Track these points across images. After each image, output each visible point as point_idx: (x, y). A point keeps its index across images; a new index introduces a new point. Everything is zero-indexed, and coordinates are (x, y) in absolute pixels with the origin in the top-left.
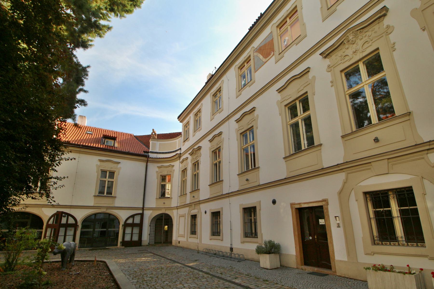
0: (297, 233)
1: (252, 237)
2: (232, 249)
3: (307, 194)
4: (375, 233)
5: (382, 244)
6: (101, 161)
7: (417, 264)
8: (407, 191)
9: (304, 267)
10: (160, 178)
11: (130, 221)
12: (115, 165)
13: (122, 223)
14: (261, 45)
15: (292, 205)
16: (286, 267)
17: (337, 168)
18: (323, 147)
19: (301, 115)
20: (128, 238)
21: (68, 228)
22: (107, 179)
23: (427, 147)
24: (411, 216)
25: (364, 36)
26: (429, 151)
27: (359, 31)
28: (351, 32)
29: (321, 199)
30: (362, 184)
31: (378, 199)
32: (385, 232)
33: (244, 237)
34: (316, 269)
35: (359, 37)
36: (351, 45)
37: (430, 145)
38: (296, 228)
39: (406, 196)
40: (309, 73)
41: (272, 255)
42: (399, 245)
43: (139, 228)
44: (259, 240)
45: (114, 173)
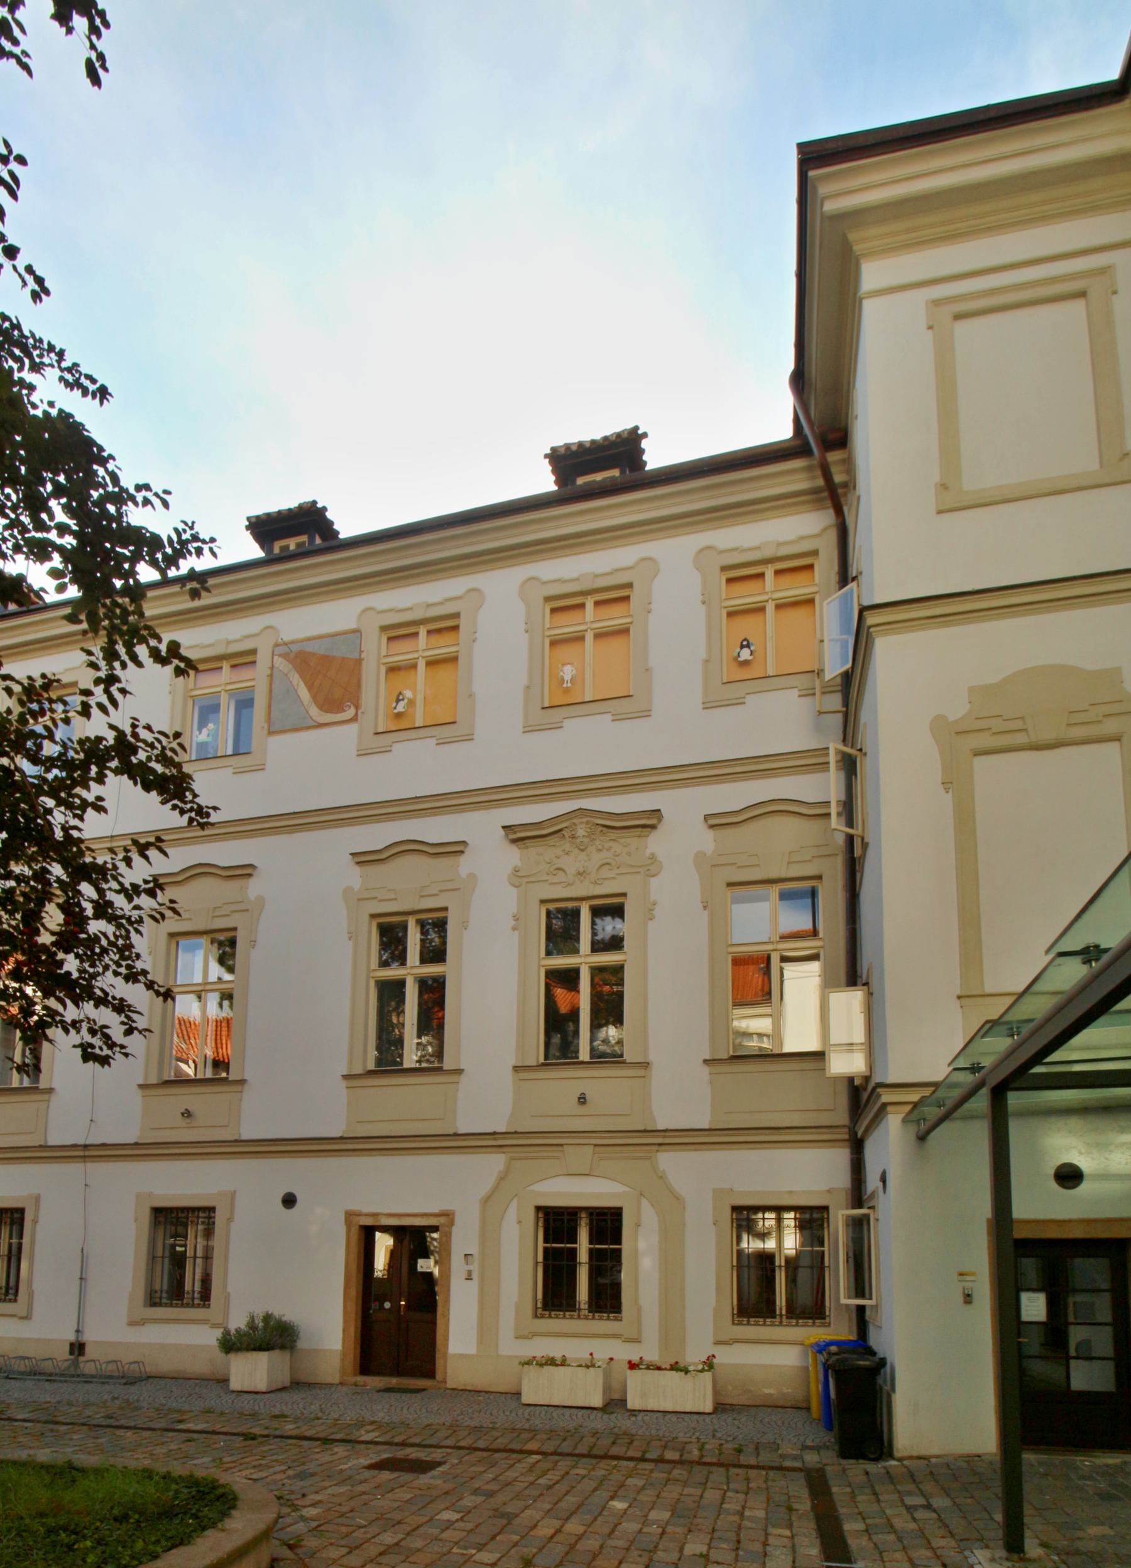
0: (353, 1292)
1: (182, 1306)
2: (78, 1348)
3: (400, 1190)
4: (540, 1295)
5: (550, 1317)
7: (603, 1350)
8: (612, 1214)
9: (361, 1379)
14: (311, 648)
16: (309, 1385)
18: (463, 1078)
19: (413, 969)
22: (584, 959)
23: (660, 1141)
24: (565, 1263)
25: (607, 845)
26: (663, 1148)
27: (601, 828)
28: (585, 820)
29: (436, 1211)
31: (557, 1223)
32: (556, 1294)
33: (145, 1306)
34: (394, 1381)
35: (597, 842)
36: (576, 851)
37: (664, 1137)
38: (354, 1280)
39: (608, 1223)
40: (463, 859)
41: (276, 1354)
42: (579, 1317)
43: (1105, 1262)
44: (214, 1311)
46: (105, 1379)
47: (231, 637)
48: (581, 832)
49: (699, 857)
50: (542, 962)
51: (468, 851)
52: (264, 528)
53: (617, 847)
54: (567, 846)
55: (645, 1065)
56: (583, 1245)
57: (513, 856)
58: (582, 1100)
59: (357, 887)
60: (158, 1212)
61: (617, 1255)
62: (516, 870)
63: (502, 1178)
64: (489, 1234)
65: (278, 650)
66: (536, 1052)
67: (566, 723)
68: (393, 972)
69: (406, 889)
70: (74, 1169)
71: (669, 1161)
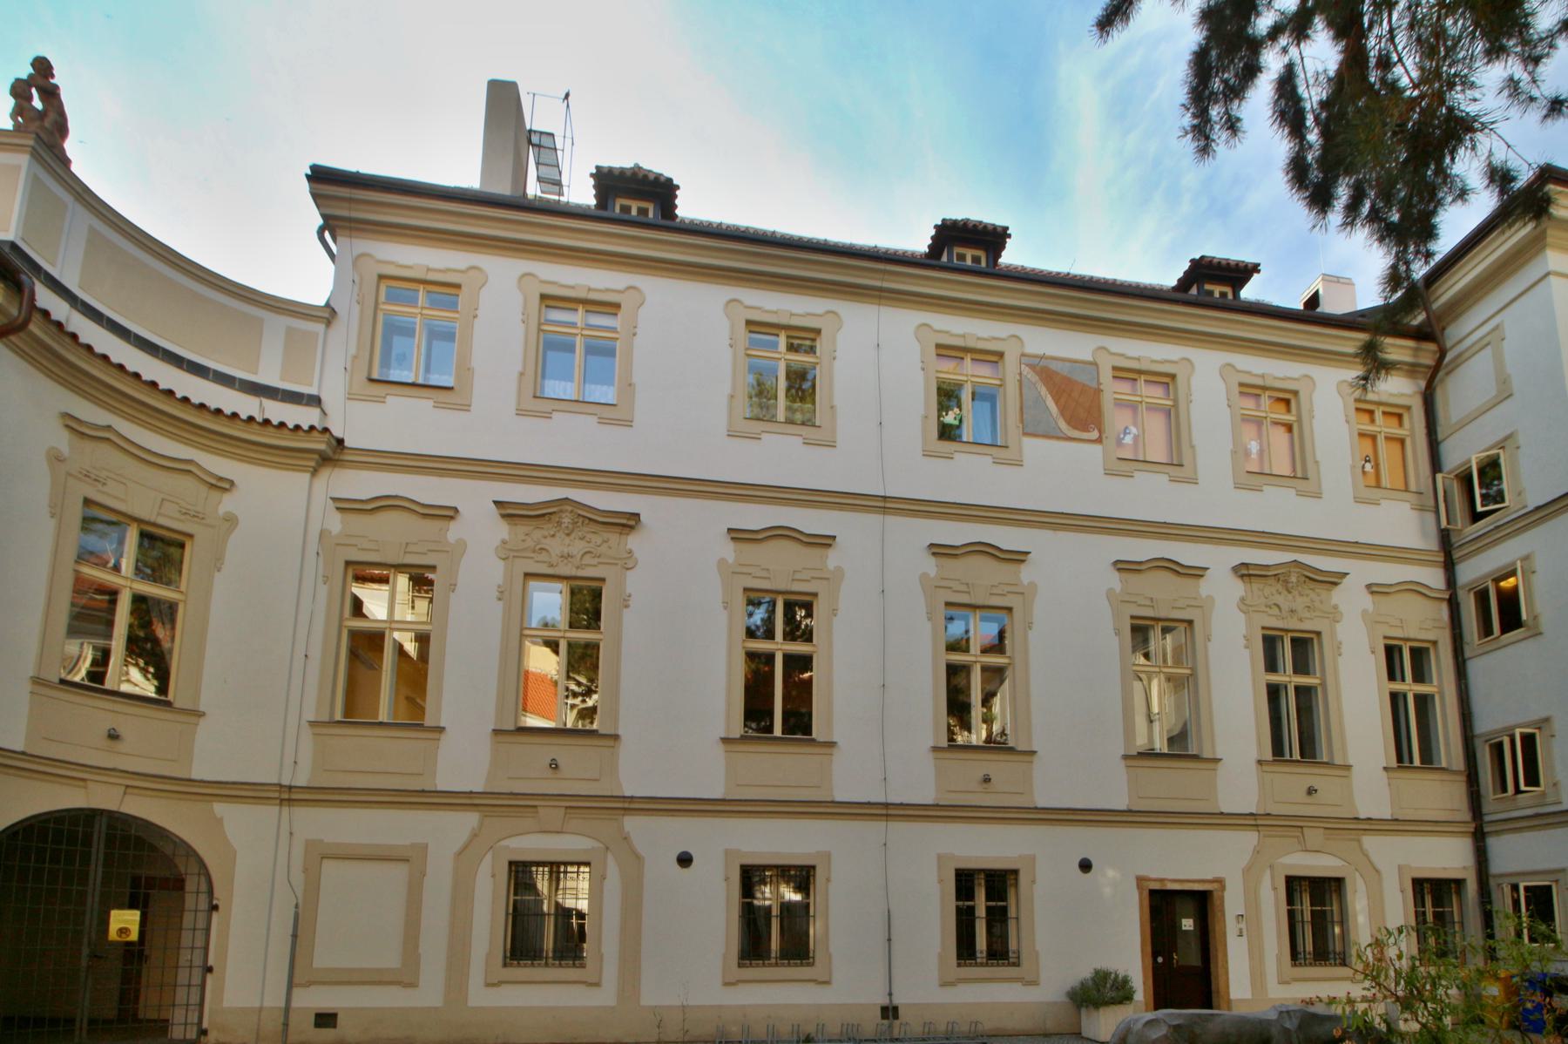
3: (1183, 860)
14: (1054, 366)
15: (1140, 880)
17: (1250, 821)
18: (1035, 758)
21: (141, 1016)
29: (1209, 877)
30: (514, 843)
40: (453, 524)
42: (547, 965)
47: (795, 311)
48: (566, 520)
51: (459, 518)
52: (610, 183)
53: (597, 539)
55: (616, 737)
56: (981, 904)
57: (502, 530)
58: (987, 780)
59: (731, 561)
61: (1004, 910)
62: (1242, 600)
63: (475, 835)
65: (1024, 360)
67: (1136, 474)
69: (782, 569)
71: (1371, 842)
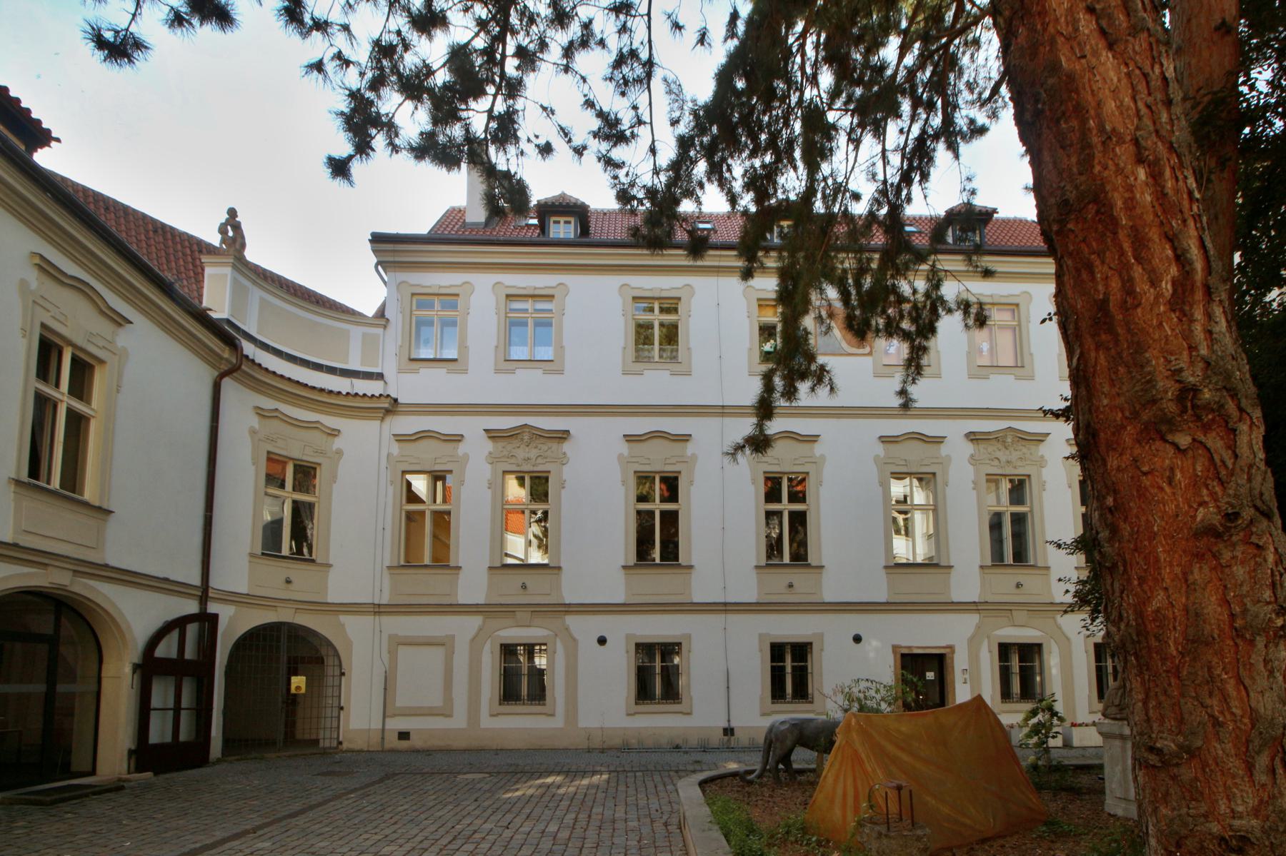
6: (46, 268)
10: (632, 481)
11: (166, 649)
12: (802, 448)
13: (134, 654)
15: (895, 648)
20: (159, 732)
22: (785, 506)
31: (777, 651)
45: (547, 479)
46: (347, 751)
49: (620, 456)
50: (680, 506)
54: (1000, 446)
55: (559, 568)
56: (788, 664)
58: (791, 586)
60: (638, 645)
62: (972, 456)
64: (974, 658)
66: (632, 559)
68: (774, 507)
69: (658, 459)
70: (716, 620)
71: (572, 621)
